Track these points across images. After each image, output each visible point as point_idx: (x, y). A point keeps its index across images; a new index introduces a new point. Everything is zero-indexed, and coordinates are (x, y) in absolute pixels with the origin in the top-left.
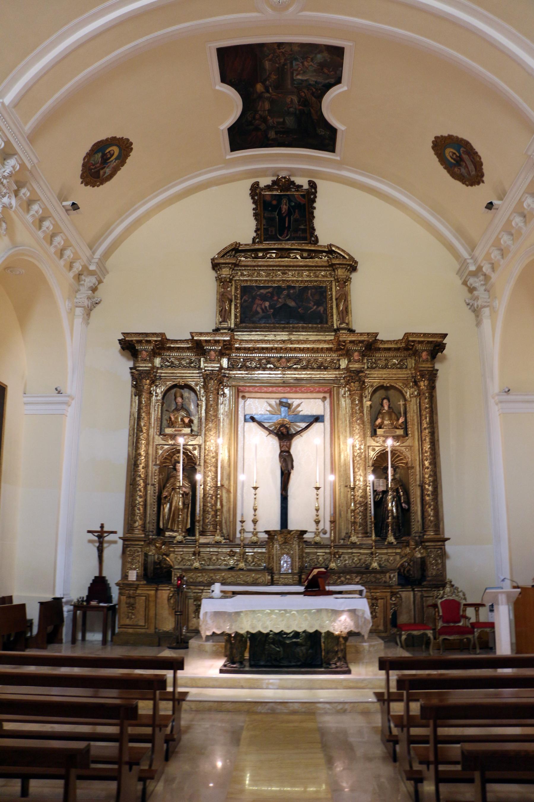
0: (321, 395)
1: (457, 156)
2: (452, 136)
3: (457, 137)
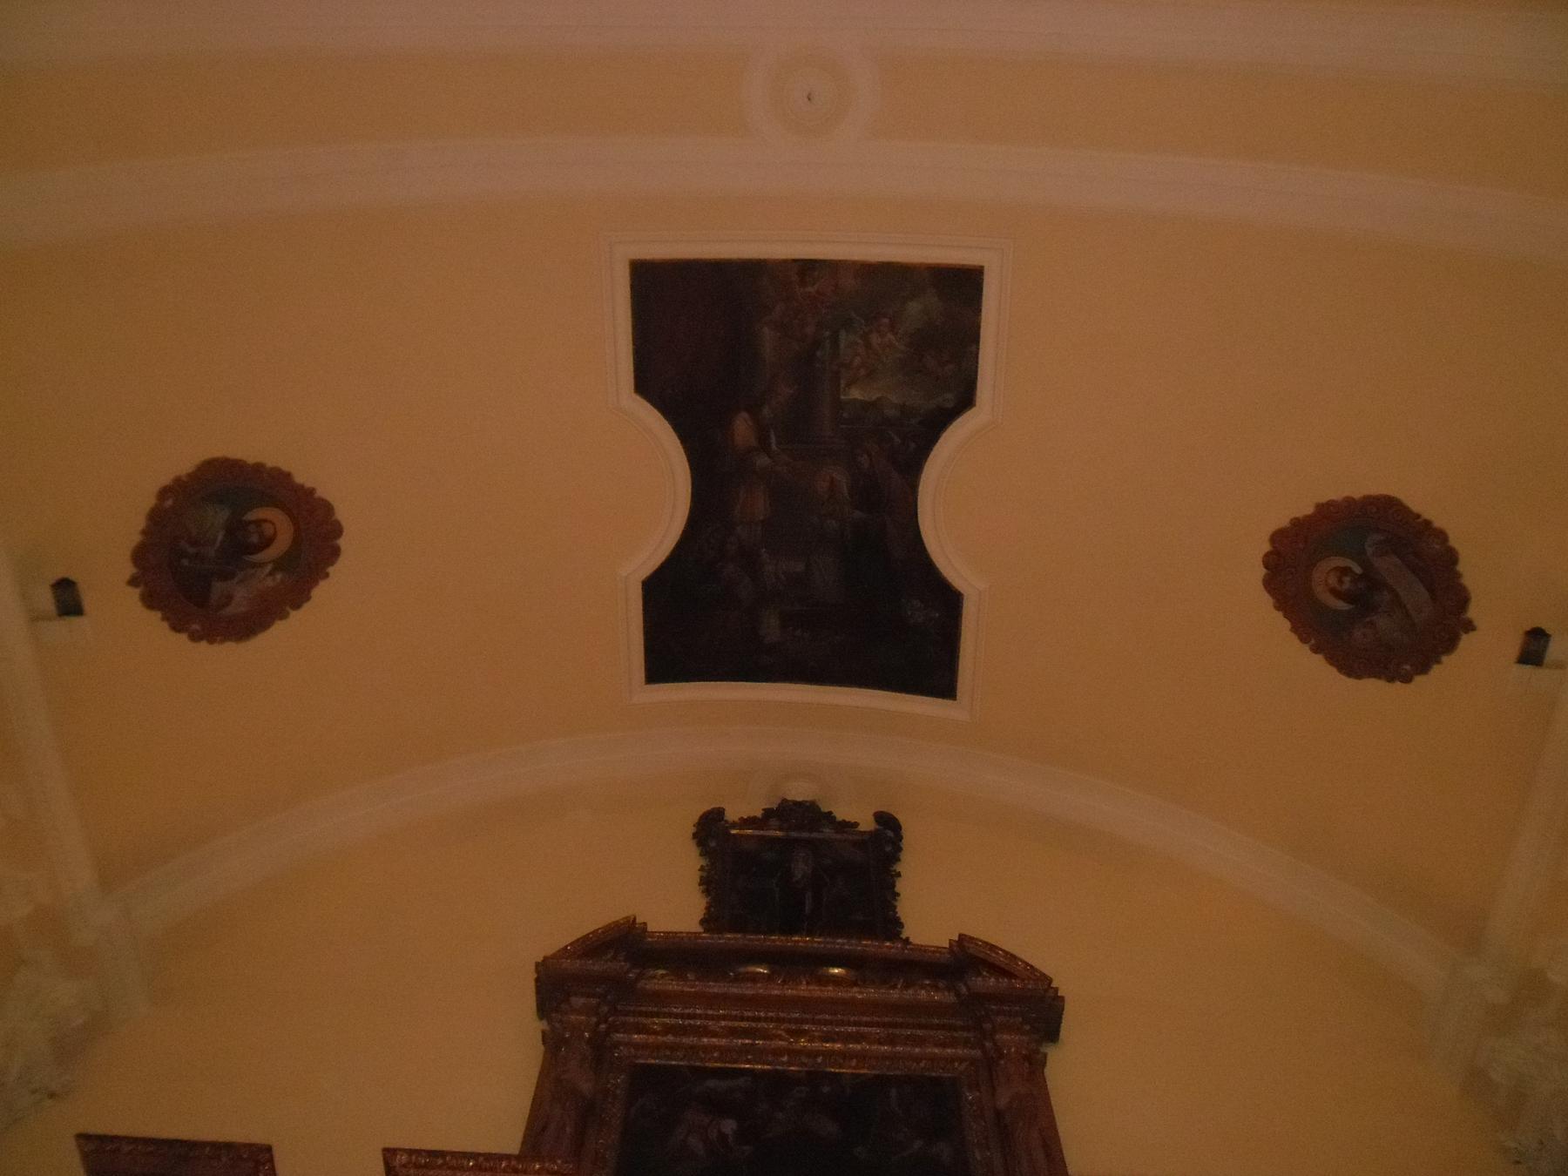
2: (1330, 504)
3: (1349, 501)
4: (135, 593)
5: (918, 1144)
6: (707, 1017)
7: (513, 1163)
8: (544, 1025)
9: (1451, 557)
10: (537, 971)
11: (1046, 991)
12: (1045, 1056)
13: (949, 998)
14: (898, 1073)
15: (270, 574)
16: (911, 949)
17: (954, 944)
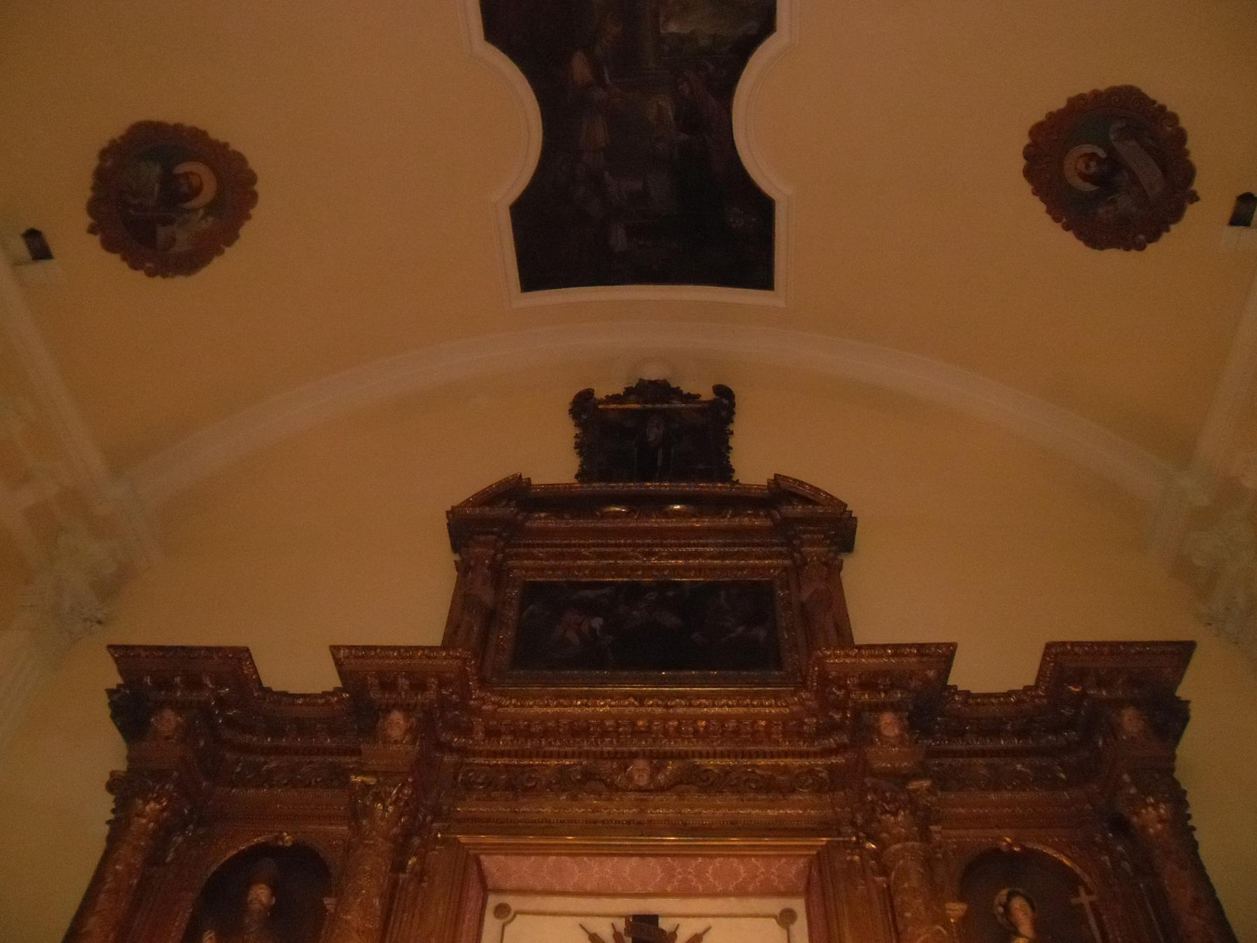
0: (775, 905)
1: (1100, 161)
2: (1081, 97)
3: (1096, 94)
4: (96, 240)
5: (740, 629)
6: (580, 545)
7: (426, 652)
8: (457, 557)
9: (1180, 137)
10: (448, 517)
11: (842, 513)
12: (842, 561)
13: (768, 523)
14: (726, 579)
15: (204, 217)
16: (738, 488)
17: (772, 482)
